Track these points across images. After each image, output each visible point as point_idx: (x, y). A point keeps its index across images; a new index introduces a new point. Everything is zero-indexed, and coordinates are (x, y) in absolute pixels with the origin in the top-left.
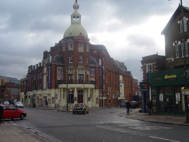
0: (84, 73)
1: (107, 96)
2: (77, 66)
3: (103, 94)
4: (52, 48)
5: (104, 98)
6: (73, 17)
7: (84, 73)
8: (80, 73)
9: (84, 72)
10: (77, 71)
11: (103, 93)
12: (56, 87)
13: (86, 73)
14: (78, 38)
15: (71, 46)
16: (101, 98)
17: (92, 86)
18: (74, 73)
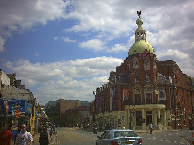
0: (152, 93)
1: (181, 116)
2: (144, 85)
3: (175, 115)
4: (118, 68)
5: (177, 119)
6: (136, 34)
7: (152, 93)
8: (147, 93)
9: (152, 91)
10: (144, 90)
11: (175, 113)
12: (123, 109)
13: (154, 92)
14: (143, 55)
15: (136, 64)
16: (173, 120)
17: (164, 106)
18: (141, 93)
